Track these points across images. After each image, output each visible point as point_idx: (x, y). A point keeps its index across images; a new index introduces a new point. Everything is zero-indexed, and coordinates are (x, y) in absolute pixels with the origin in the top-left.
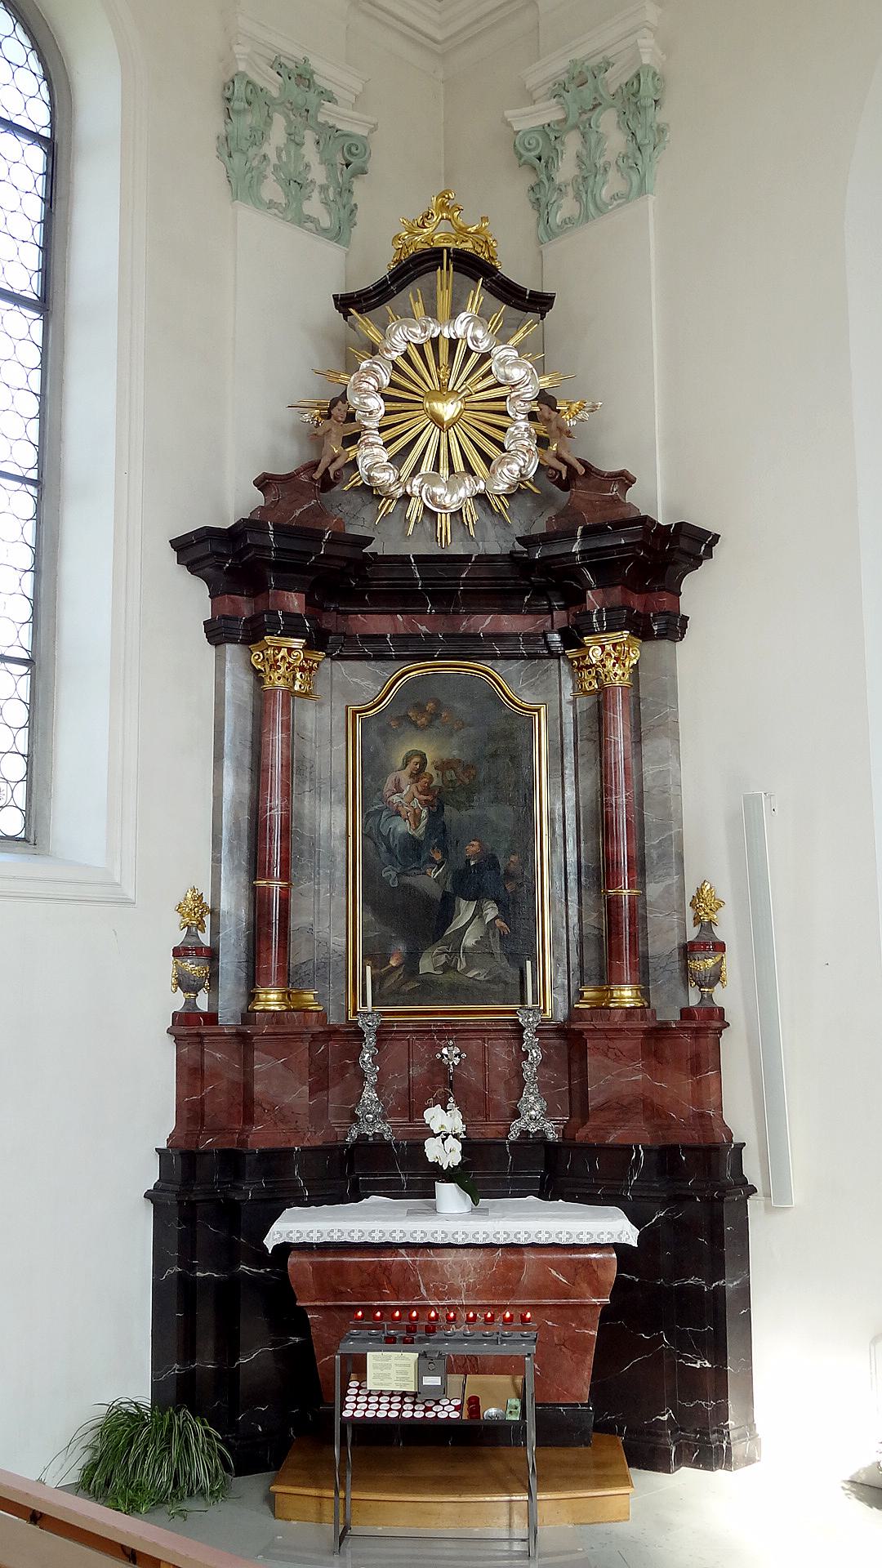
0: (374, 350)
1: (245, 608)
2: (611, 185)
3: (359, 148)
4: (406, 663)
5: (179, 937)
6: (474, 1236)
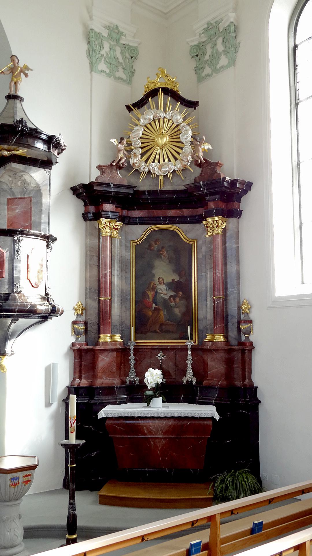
0: (184, 119)
1: (92, 209)
2: (223, 61)
3: (135, 52)
4: (153, 225)
5: (74, 318)
6: (208, 415)
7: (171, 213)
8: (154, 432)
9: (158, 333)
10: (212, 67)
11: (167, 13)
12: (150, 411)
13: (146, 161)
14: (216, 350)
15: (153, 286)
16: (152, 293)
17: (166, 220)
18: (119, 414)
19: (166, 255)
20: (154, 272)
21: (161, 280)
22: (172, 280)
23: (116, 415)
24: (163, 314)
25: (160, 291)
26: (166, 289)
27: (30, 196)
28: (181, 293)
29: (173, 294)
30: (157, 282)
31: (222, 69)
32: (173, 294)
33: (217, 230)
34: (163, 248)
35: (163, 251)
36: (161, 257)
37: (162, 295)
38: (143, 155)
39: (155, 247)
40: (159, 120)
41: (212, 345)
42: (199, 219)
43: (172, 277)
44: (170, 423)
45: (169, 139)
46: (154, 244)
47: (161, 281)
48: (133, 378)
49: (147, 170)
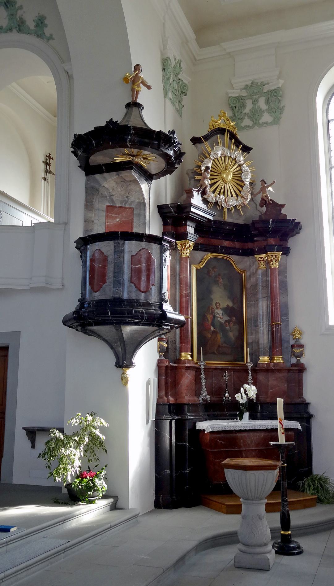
2: (267, 118)
7: (226, 243)
8: (249, 444)
9: (217, 355)
10: (254, 120)
11: (199, 60)
12: (248, 424)
13: (214, 192)
14: (279, 370)
15: (211, 310)
16: (211, 316)
17: (223, 250)
18: (224, 428)
19: (222, 282)
20: (212, 296)
21: (218, 305)
22: (227, 305)
23: (221, 429)
24: (220, 336)
25: (217, 315)
26: (222, 313)
27: (132, 207)
28: (234, 318)
29: (227, 318)
30: (215, 307)
31: (265, 125)
32: (227, 318)
33: (276, 264)
34: (219, 275)
35: (219, 278)
36: (218, 284)
37: (219, 319)
38: (212, 185)
39: (213, 274)
40: (225, 157)
41: (274, 366)
42: (249, 253)
43: (226, 303)
44: (262, 435)
45: (232, 178)
46: (211, 270)
47: (218, 306)
48: (205, 396)
49: (214, 201)
